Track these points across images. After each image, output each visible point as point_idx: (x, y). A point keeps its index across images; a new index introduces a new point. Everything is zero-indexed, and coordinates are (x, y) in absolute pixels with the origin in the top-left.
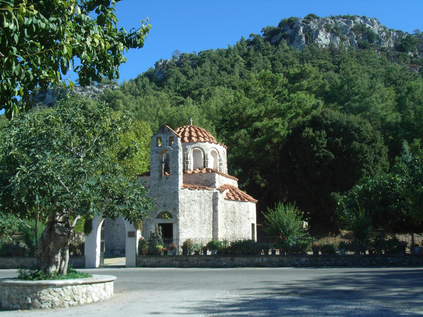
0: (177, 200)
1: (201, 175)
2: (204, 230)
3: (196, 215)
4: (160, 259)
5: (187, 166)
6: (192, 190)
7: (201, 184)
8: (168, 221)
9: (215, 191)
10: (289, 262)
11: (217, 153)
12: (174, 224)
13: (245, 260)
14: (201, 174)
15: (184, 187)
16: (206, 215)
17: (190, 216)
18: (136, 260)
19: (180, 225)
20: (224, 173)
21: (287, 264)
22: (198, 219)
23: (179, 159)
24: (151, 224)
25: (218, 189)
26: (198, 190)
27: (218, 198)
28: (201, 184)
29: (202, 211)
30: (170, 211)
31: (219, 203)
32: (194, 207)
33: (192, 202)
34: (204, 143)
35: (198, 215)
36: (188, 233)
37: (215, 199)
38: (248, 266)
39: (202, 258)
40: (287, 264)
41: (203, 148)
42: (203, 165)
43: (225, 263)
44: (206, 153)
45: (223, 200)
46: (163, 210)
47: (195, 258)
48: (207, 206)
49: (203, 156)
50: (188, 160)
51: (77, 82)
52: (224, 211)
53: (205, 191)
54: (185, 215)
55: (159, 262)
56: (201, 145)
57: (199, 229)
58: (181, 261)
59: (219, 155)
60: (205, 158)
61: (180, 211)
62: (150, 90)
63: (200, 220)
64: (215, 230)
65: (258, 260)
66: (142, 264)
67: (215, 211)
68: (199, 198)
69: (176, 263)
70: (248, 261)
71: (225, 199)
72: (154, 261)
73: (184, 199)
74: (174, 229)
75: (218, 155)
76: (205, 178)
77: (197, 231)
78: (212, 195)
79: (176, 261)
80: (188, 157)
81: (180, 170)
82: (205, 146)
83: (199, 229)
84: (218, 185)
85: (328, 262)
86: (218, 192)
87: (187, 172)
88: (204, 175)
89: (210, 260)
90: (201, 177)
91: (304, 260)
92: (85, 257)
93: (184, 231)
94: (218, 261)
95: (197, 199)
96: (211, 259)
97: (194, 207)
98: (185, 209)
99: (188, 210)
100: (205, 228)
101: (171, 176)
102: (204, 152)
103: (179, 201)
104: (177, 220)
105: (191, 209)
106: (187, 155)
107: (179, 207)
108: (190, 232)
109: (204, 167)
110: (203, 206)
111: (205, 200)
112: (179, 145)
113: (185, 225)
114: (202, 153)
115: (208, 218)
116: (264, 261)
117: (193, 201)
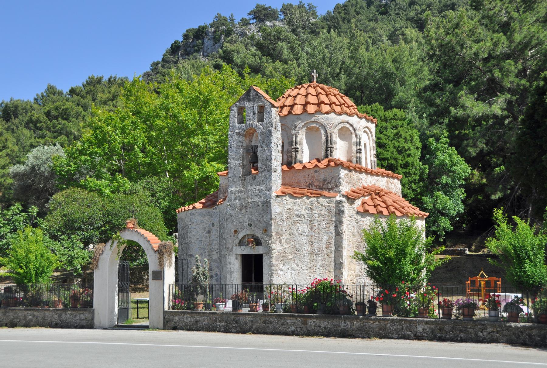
0: (269, 215)
1: (316, 172)
2: (318, 267)
3: (304, 240)
4: (198, 318)
5: (296, 156)
6: (296, 198)
7: (316, 186)
8: (259, 250)
9: (338, 198)
10: (395, 330)
11: (353, 131)
12: (264, 256)
13: (324, 324)
14: (316, 169)
15: (283, 193)
16: (322, 241)
17: (293, 243)
18: (164, 318)
19: (273, 258)
20: (369, 167)
21: (392, 334)
22: (306, 248)
23: (273, 145)
24: (229, 255)
25: (343, 196)
26: (308, 197)
27: (343, 212)
28: (316, 186)
29: (314, 234)
30: (259, 234)
31: (346, 220)
32: (300, 227)
33: (296, 219)
34: (326, 115)
35: (306, 241)
36: (289, 271)
37: (339, 213)
38: (328, 334)
39: (258, 319)
40: (392, 334)
41: (325, 123)
42: (323, 153)
43: (293, 328)
44: (329, 131)
45: (353, 213)
46: (248, 232)
47: (248, 318)
48: (324, 224)
49: (323, 138)
50: (298, 146)
51: (251, 17)
52: (356, 233)
53: (321, 200)
54: (283, 241)
55: (197, 322)
56: (321, 118)
57: (309, 265)
58: (227, 322)
59: (356, 136)
60: (328, 142)
61: (274, 234)
62: (362, 22)
63: (309, 249)
64: (339, 266)
65: (345, 324)
66: (172, 324)
67: (338, 234)
68: (309, 212)
69: (221, 324)
70: (329, 326)
71: (358, 213)
72: (189, 320)
73: (281, 213)
74: (264, 264)
75: (354, 136)
76: (322, 177)
77: (305, 268)
78: (333, 205)
79: (220, 321)
80: (298, 139)
81: (277, 162)
82: (327, 119)
83: (309, 265)
84: (345, 188)
85: (462, 335)
86: (344, 199)
87: (295, 166)
88: (322, 171)
89: (271, 323)
90: (316, 174)
91: (421, 329)
92: (93, 310)
93: (281, 267)
94: (282, 325)
95: (304, 212)
96: (272, 320)
97: (300, 227)
98: (284, 230)
99: (288, 232)
100: (320, 263)
101: (260, 175)
102: (326, 132)
103: (273, 216)
104: (269, 250)
105: (294, 231)
106: (296, 137)
107: (273, 227)
108: (293, 270)
109: (327, 156)
110: (316, 224)
111: (320, 214)
112: (274, 120)
113: (283, 257)
114: (323, 132)
115: (324, 245)
116: (354, 327)
117: (298, 216)
